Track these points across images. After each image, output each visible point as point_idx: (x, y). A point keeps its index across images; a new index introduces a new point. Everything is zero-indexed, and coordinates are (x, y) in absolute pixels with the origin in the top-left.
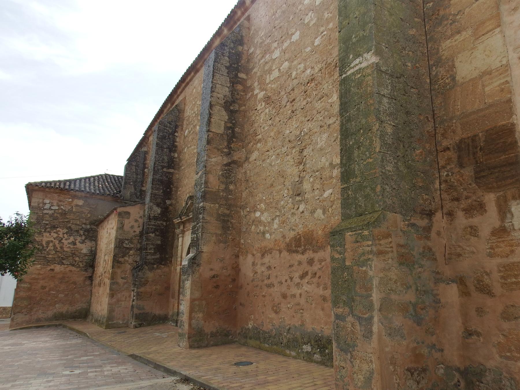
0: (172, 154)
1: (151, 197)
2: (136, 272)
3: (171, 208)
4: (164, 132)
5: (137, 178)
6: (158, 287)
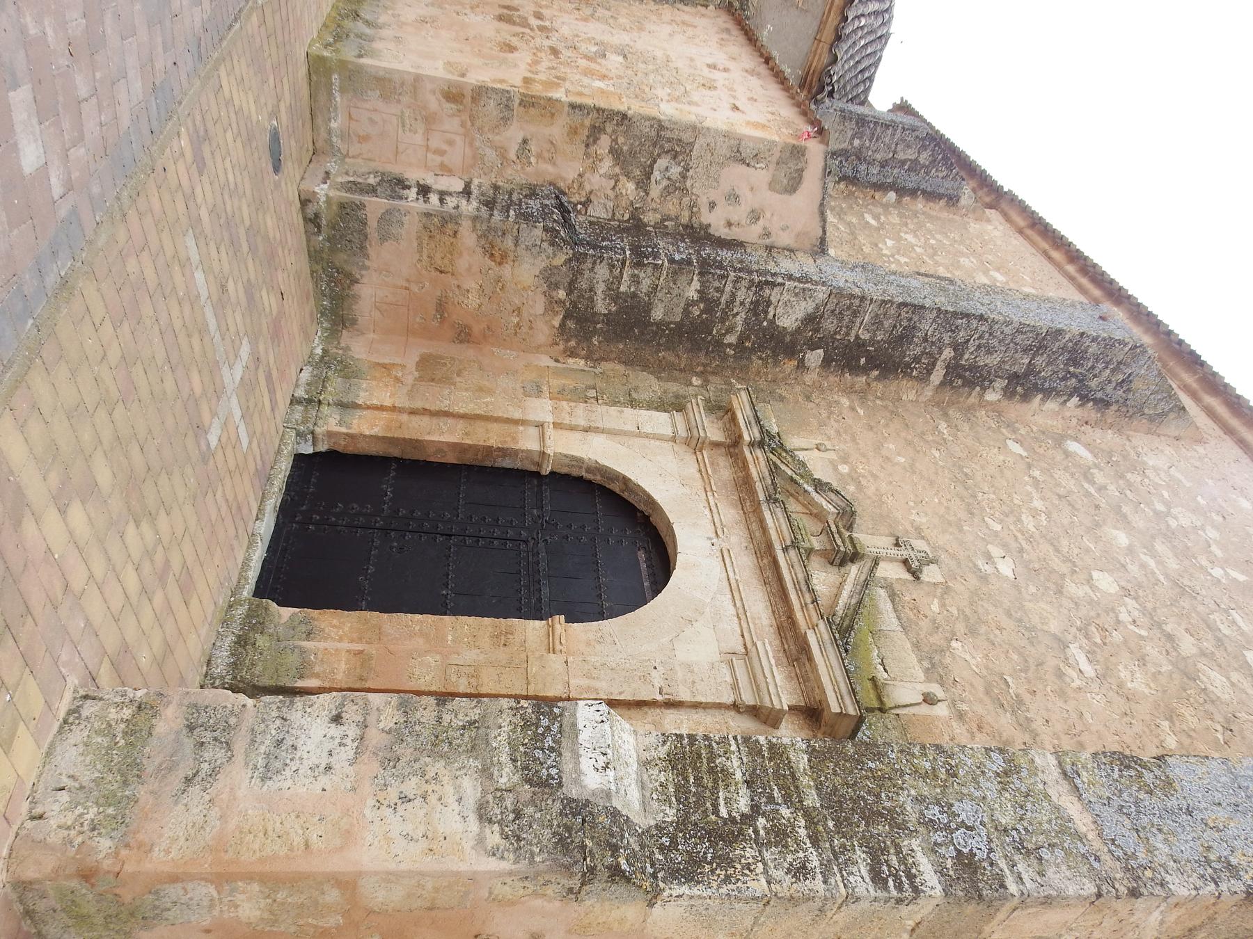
0: (1000, 384)
1: (852, 296)
2: (545, 213)
3: (790, 365)
4: (1097, 360)
5: (871, 163)
6: (473, 301)
